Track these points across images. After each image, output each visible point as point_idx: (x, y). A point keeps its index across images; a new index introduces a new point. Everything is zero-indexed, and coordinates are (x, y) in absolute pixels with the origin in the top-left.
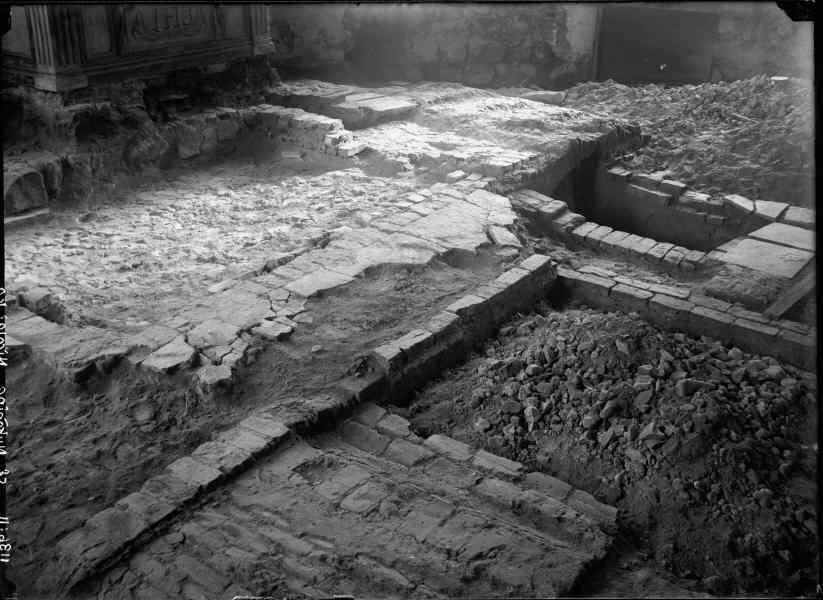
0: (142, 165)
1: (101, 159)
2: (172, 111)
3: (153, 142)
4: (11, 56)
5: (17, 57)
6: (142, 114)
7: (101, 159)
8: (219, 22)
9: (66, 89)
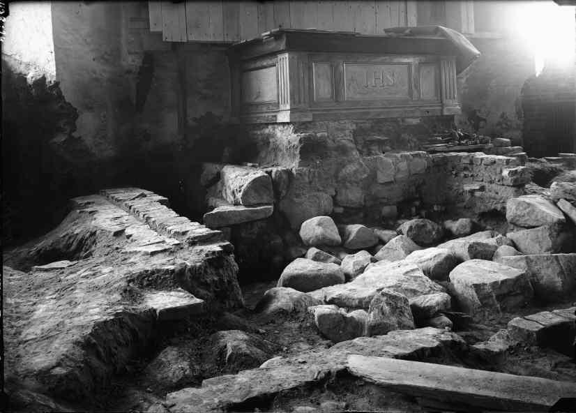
0: (348, 184)
1: (316, 174)
2: (375, 148)
3: (357, 167)
4: (263, 104)
5: (268, 104)
6: (351, 145)
7: (316, 174)
8: (416, 87)
9: (297, 120)
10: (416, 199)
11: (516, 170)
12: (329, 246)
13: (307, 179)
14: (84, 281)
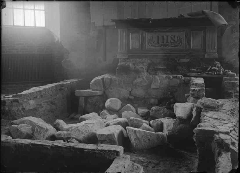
10: (171, 98)
11: (195, 89)
12: (111, 110)
13: (117, 83)
14: (211, 119)
